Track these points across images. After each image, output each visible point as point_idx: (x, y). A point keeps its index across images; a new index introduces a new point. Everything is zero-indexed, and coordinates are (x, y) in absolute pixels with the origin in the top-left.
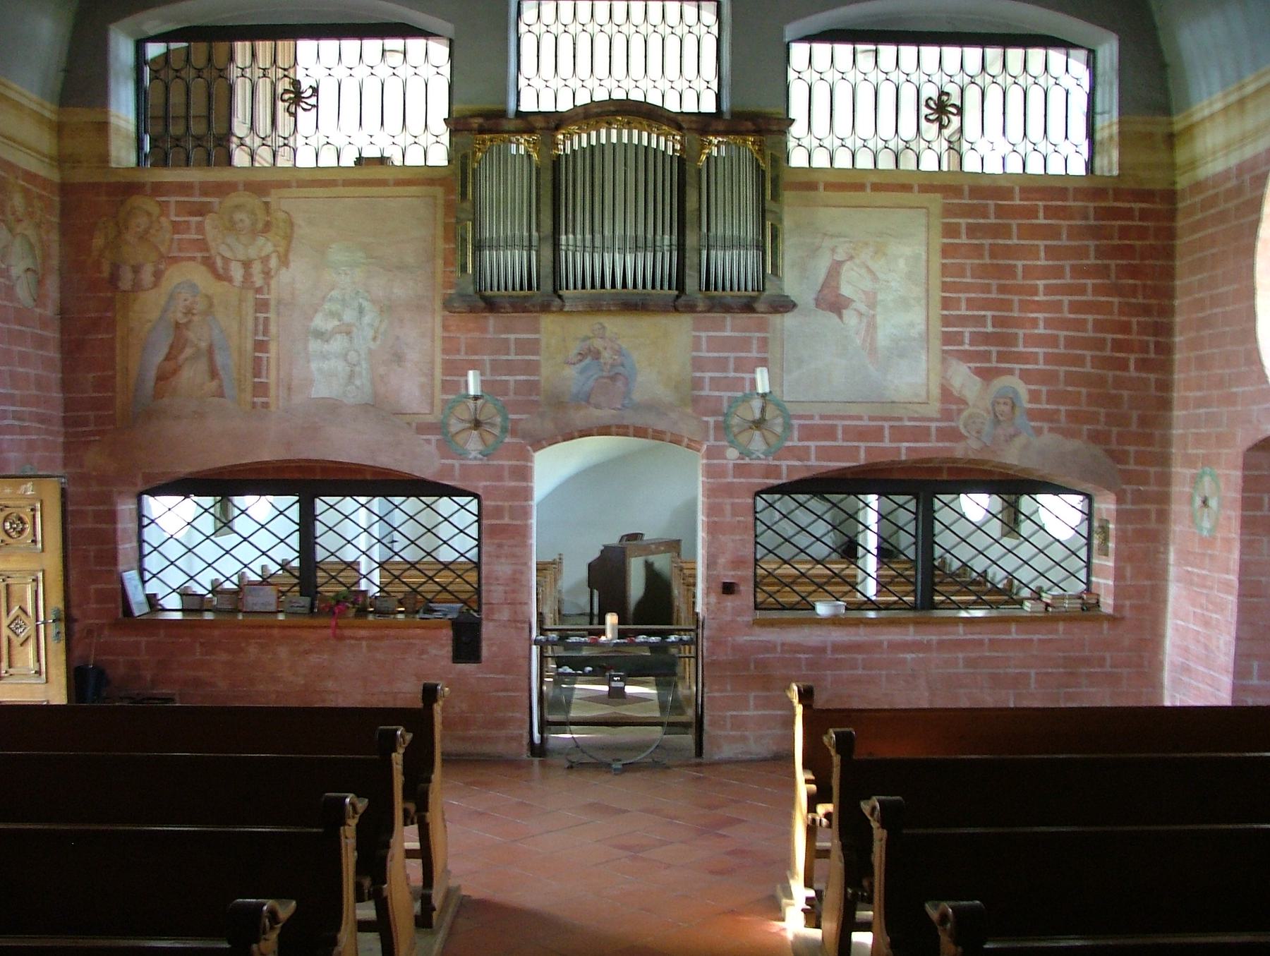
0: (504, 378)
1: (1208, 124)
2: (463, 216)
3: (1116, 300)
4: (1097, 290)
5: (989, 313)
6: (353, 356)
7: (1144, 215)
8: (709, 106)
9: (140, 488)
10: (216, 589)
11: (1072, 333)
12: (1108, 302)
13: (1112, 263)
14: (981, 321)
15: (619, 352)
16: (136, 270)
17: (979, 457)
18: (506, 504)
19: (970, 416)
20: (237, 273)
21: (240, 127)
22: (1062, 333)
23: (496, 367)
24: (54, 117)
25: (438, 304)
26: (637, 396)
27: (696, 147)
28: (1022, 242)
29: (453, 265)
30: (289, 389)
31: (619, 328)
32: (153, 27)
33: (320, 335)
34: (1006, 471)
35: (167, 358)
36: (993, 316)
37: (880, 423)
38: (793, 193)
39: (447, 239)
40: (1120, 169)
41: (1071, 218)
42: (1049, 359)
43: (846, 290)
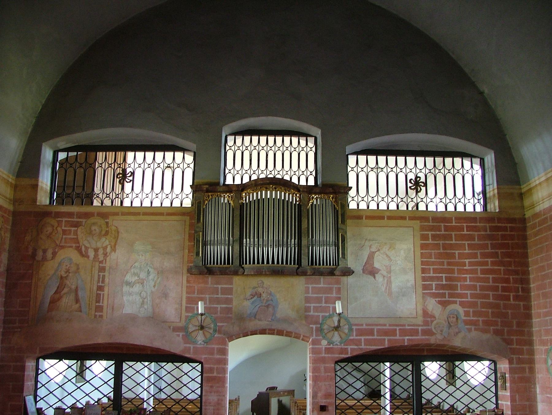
0: (215, 306)
1: (539, 188)
3: (502, 268)
4: (493, 263)
5: (444, 275)
6: (144, 294)
7: (512, 229)
8: (311, 182)
9: (38, 355)
10: (73, 407)
11: (483, 284)
12: (498, 269)
15: (270, 294)
16: (45, 251)
17: (442, 343)
18: (215, 366)
19: (437, 324)
20: (91, 254)
21: (97, 190)
22: (478, 284)
23: (211, 301)
24: (13, 182)
25: (185, 271)
26: (278, 315)
27: (306, 199)
28: (458, 242)
29: (192, 252)
30: (113, 309)
31: (269, 282)
33: (128, 284)
34: (454, 350)
35: (56, 292)
37: (395, 328)
39: (190, 240)
41: (480, 231)
42: (472, 296)
43: (377, 265)
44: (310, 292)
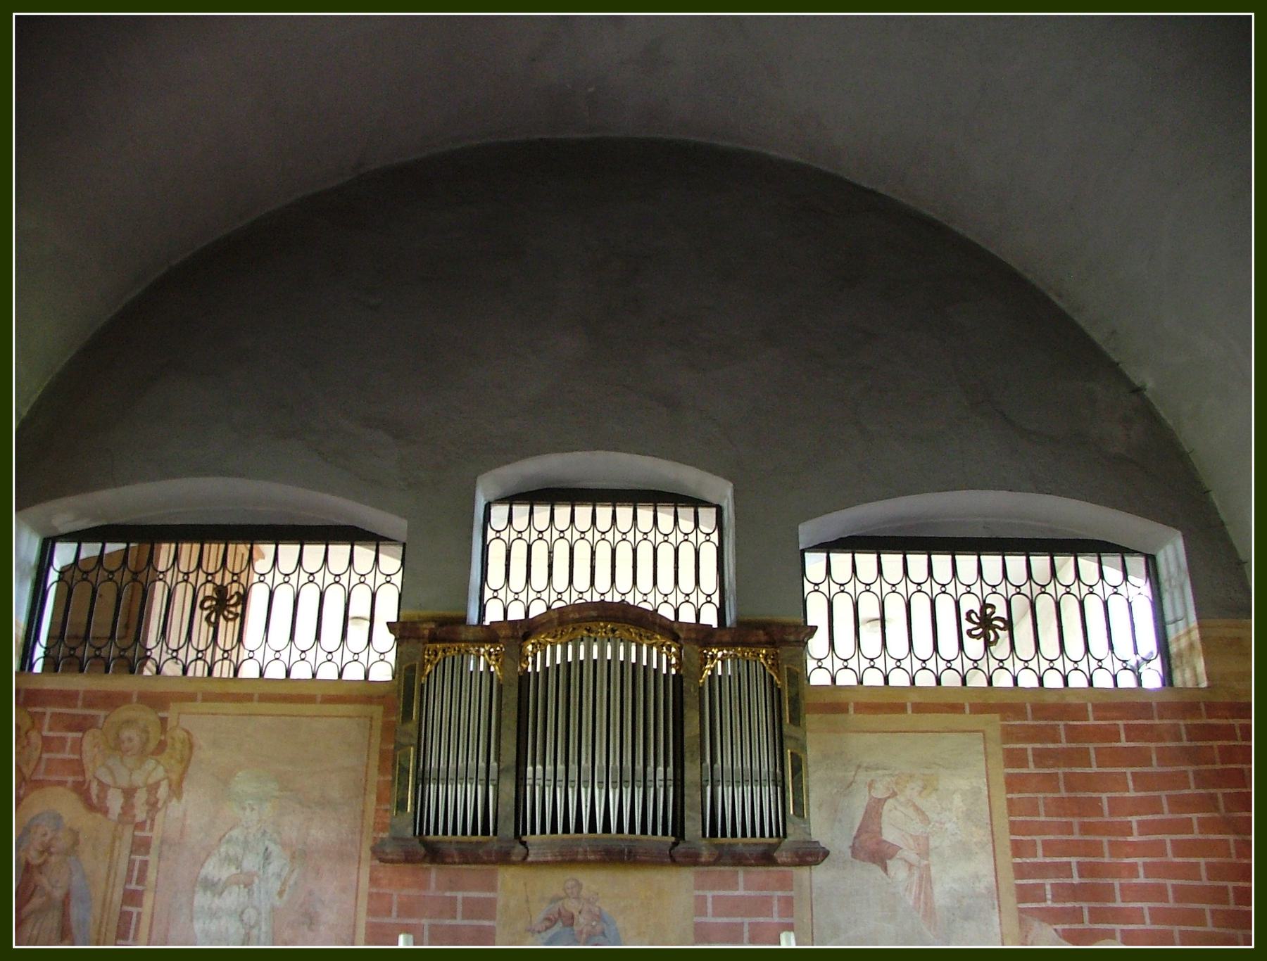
2: (404, 740)
4: (1204, 825)
5: (1073, 860)
13: (1219, 792)
14: (1064, 869)
15: (600, 917)
20: (115, 802)
22: (1170, 883)
25: (366, 853)
27: (696, 659)
32: (65, 522)
33: (211, 886)
36: (1078, 863)
38: (816, 717)
39: (381, 770)
40: (1208, 678)
42: (1157, 916)
44: (710, 910)
